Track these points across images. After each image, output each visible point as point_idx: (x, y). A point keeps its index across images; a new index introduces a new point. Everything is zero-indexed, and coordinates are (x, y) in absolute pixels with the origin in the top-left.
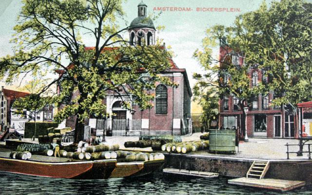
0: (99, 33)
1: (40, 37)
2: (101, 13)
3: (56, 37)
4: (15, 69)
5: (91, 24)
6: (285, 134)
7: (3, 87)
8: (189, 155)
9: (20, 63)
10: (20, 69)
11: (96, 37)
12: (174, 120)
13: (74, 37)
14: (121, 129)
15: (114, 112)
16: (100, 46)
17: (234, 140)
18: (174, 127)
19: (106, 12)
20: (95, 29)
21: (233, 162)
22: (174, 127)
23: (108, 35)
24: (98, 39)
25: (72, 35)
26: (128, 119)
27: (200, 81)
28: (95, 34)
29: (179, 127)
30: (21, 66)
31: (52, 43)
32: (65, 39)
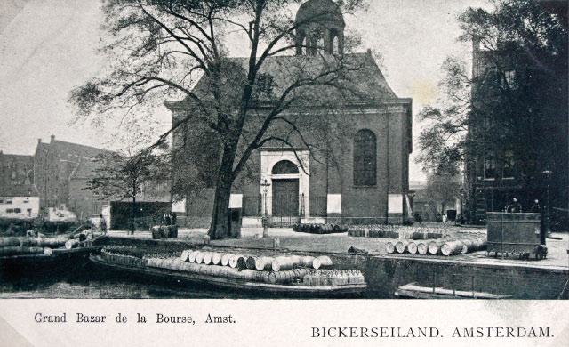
0: (255, 32)
1: (151, 45)
3: (179, 39)
4: (107, 98)
7: (40, 140)
8: (455, 260)
14: (203, 227)
15: (273, 180)
16: (259, 55)
17: (538, 232)
22: (389, 211)
25: (210, 35)
28: (250, 33)
29: (400, 210)
31: (171, 52)
32: (198, 44)
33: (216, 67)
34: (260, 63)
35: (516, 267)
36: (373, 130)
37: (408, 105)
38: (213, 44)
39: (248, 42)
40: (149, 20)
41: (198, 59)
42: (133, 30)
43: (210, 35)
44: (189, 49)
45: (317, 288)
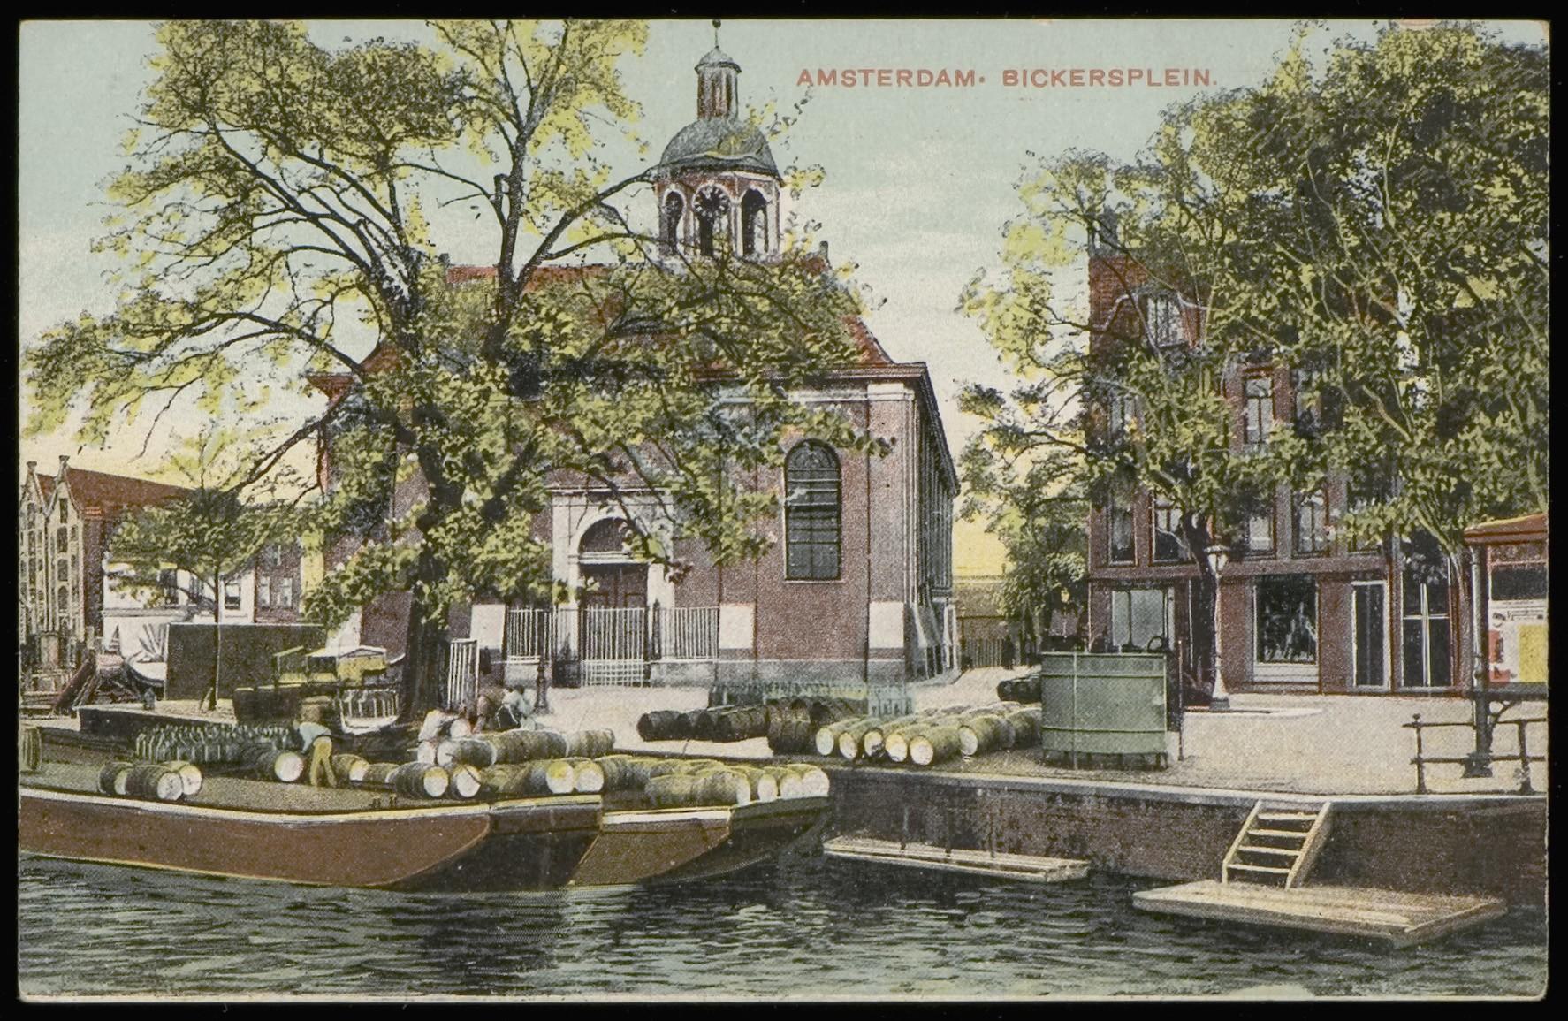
0: (509, 196)
3: (313, 218)
16: (520, 260)
17: (1161, 700)
25: (388, 209)
28: (497, 205)
29: (898, 642)
33: (405, 295)
34: (395, 208)
35: (725, 740)
36: (843, 462)
37: (920, 384)
38: (398, 228)
39: (497, 233)
40: (228, 166)
41: (361, 264)
42: (190, 190)
43: (388, 209)
44: (343, 245)
45: (1207, 792)
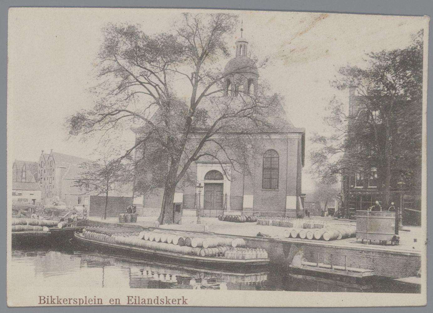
0: (196, 79)
2: (200, 52)
3: (141, 83)
5: (187, 68)
6: (325, 278)
9: (99, 118)
10: (97, 126)
11: (192, 84)
12: (287, 197)
13: (165, 85)
17: (393, 225)
18: (288, 207)
19: (205, 54)
20: (192, 74)
21: (396, 254)
23: (207, 80)
24: (195, 86)
26: (226, 195)
27: (34, 219)
30: (99, 121)
31: (136, 93)
32: (155, 87)
